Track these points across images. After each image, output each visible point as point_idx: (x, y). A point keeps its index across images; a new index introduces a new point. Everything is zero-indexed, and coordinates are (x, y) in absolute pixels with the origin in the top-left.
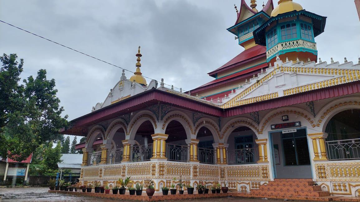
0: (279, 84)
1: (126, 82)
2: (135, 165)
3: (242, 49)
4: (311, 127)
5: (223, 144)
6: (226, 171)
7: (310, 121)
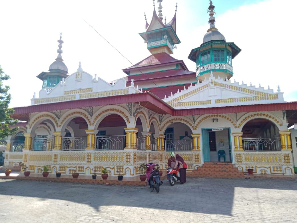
5: (162, 135)
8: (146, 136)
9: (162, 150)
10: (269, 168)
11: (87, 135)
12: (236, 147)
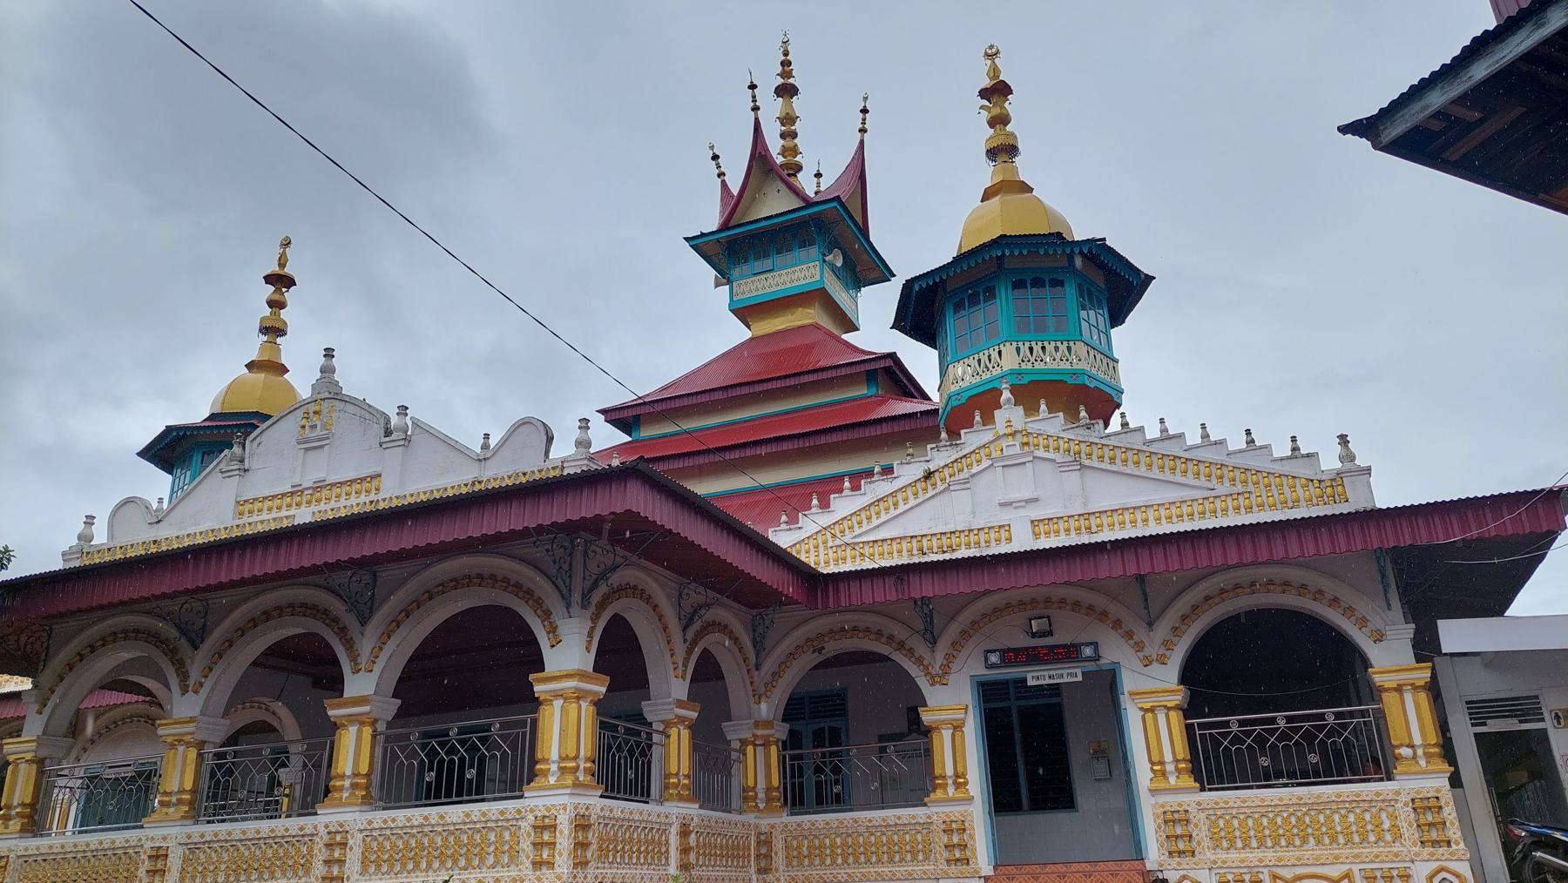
0: (1014, 495)
1: (350, 408)
2: (377, 826)
3: (739, 333)
4: (1138, 666)
5: (767, 724)
6: (778, 845)
7: (1131, 642)
8: (668, 724)
9: (769, 809)
10: (1346, 880)
11: (334, 727)
12: (1156, 763)
